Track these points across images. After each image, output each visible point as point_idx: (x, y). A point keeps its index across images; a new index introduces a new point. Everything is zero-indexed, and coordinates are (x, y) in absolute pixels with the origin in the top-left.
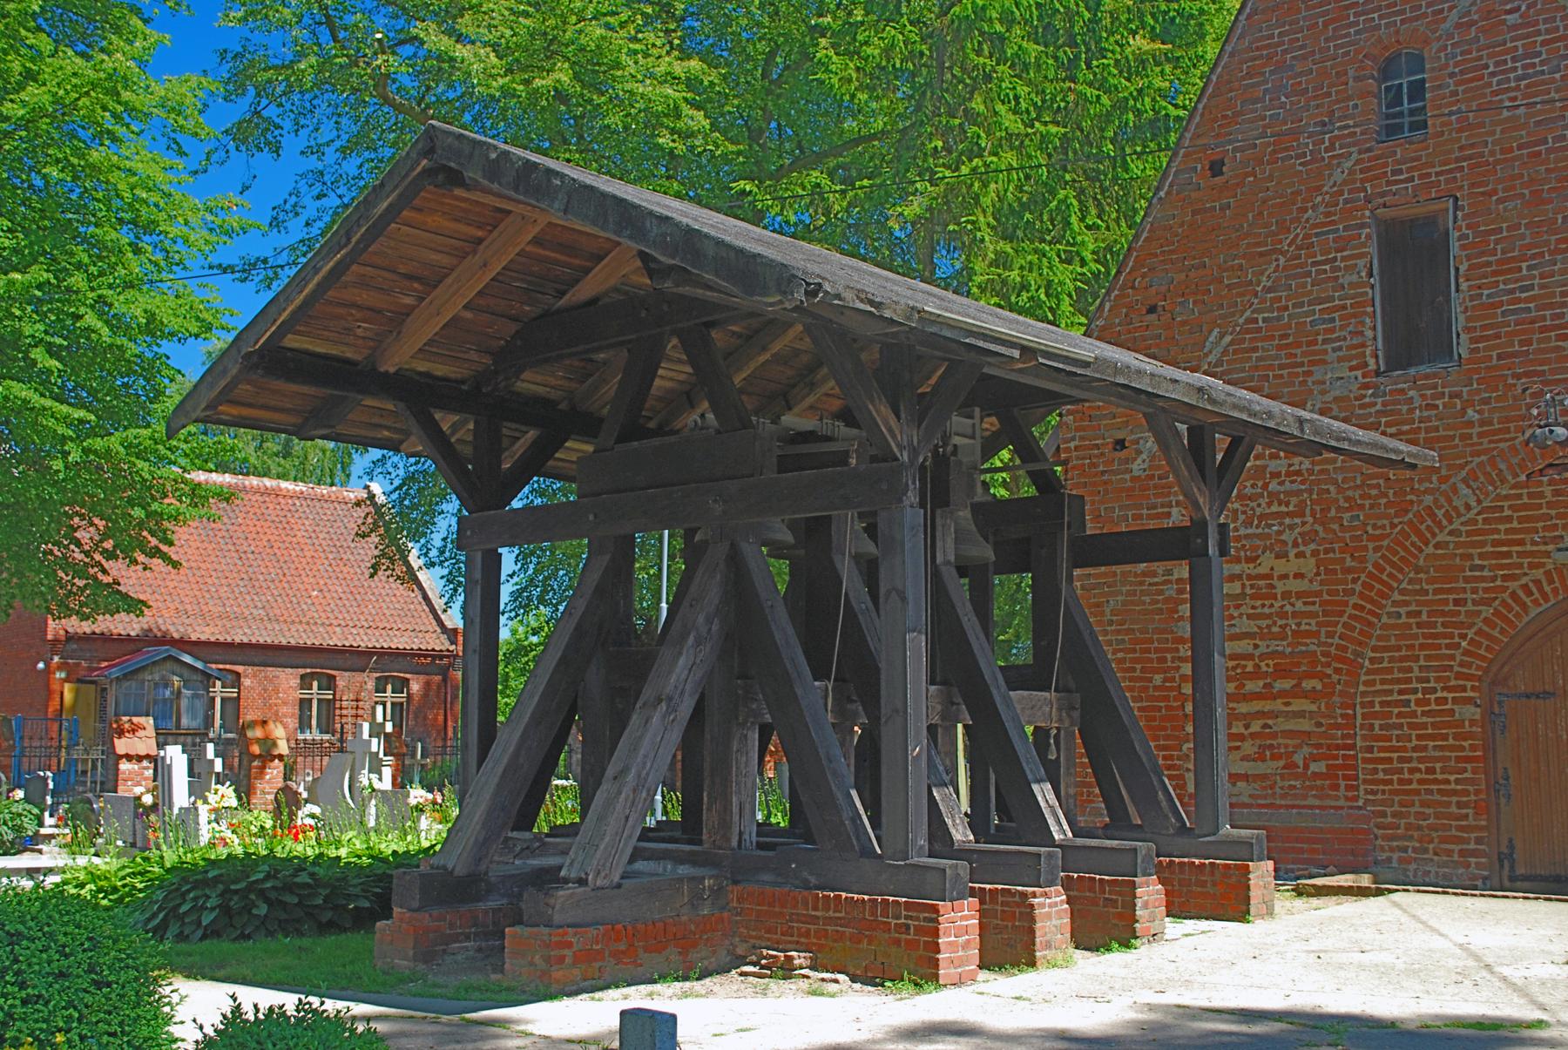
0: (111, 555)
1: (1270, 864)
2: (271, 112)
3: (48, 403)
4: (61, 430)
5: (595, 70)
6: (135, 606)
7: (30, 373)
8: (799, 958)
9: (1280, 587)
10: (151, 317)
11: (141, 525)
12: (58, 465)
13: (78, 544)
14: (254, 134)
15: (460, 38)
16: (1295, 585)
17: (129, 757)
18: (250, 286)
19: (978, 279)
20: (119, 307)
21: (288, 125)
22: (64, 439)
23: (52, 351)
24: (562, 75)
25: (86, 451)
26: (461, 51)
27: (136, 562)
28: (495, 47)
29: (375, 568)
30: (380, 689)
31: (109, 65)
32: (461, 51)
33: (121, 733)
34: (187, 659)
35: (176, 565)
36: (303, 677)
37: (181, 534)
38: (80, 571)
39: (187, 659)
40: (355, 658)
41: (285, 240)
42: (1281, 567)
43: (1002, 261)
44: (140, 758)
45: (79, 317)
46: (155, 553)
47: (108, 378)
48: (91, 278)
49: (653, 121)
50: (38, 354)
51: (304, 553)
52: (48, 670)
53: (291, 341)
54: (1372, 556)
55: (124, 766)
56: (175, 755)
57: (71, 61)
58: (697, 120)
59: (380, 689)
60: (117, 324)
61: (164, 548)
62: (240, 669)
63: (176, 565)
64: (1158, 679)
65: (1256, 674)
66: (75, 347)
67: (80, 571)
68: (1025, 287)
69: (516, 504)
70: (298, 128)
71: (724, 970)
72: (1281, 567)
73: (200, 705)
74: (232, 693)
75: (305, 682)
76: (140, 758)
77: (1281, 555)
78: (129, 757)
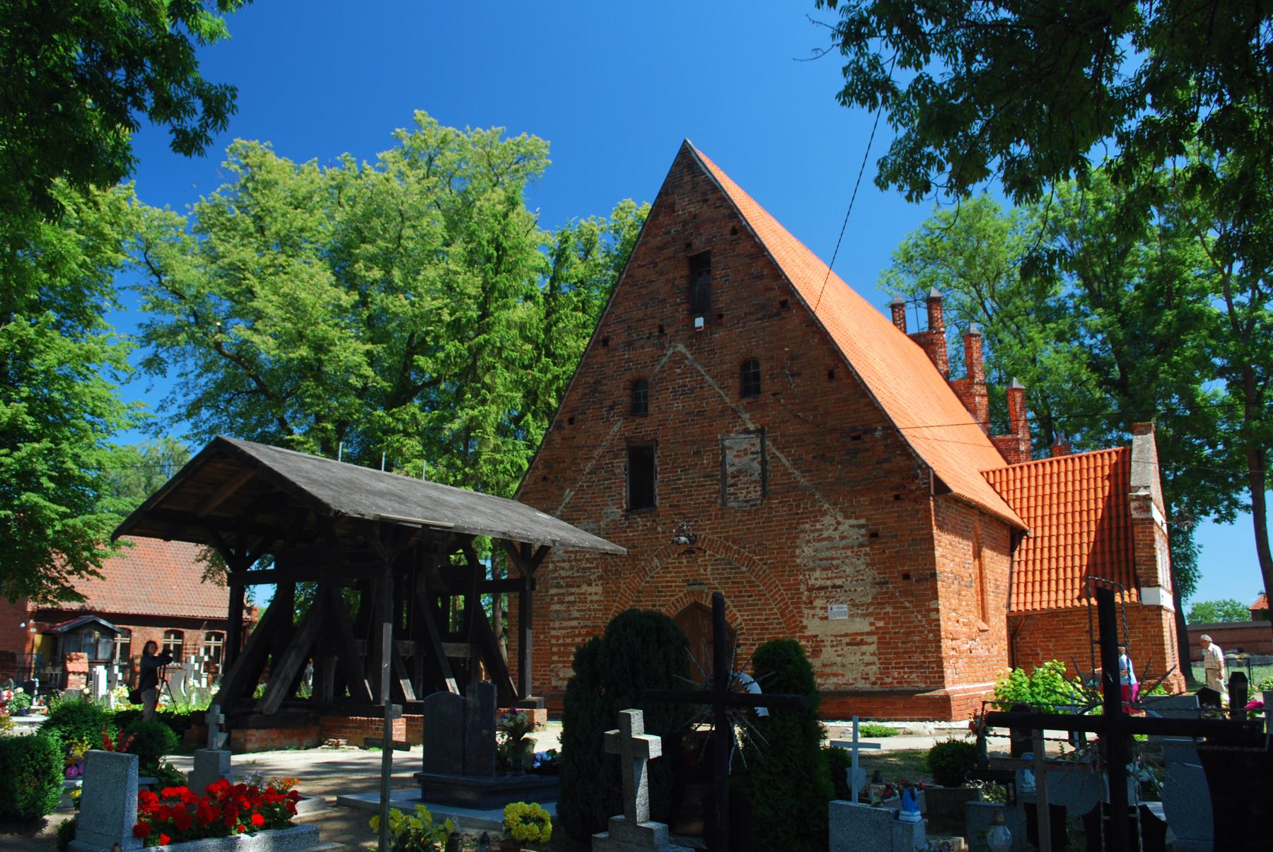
0: (70, 573)
1: (545, 711)
2: (164, 355)
3: (47, 504)
4: (53, 516)
5: (320, 346)
6: (79, 597)
7: (38, 489)
8: (342, 741)
9: (589, 598)
10: (99, 462)
11: (87, 559)
12: (49, 532)
13: (55, 567)
14: (154, 365)
15: (256, 331)
16: (595, 598)
17: (74, 673)
18: (147, 436)
19: (483, 457)
20: (84, 458)
21: (170, 361)
22: (53, 520)
23: (51, 478)
24: (304, 351)
25: (64, 525)
26: (256, 339)
27: (82, 577)
28: (274, 336)
29: (204, 578)
30: (208, 638)
31: (86, 348)
32: (256, 339)
33: (71, 660)
34: (103, 622)
35: (103, 578)
36: (166, 632)
37: (105, 563)
38: (54, 581)
39: (103, 622)
40: (194, 623)
41: (166, 415)
42: (590, 590)
43: (496, 449)
44: (79, 673)
45: (64, 462)
46: (93, 573)
47: (74, 492)
48: (71, 444)
49: (348, 370)
50: (44, 480)
51: (168, 579)
52: (27, 627)
53: (163, 506)
54: (623, 586)
55: (71, 677)
56: (101, 671)
57: (68, 343)
58: (369, 372)
59: (208, 638)
60: (83, 466)
61: (98, 570)
62: (131, 627)
63: (103, 578)
64: (542, 637)
65: (579, 635)
66: (63, 479)
67: (54, 581)
68: (502, 462)
69: (253, 568)
70: (176, 361)
71: (315, 746)
72: (590, 590)
73: (109, 647)
74: (127, 640)
75: (167, 634)
76: (79, 673)
77: (590, 585)
78: (74, 673)
